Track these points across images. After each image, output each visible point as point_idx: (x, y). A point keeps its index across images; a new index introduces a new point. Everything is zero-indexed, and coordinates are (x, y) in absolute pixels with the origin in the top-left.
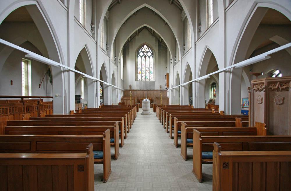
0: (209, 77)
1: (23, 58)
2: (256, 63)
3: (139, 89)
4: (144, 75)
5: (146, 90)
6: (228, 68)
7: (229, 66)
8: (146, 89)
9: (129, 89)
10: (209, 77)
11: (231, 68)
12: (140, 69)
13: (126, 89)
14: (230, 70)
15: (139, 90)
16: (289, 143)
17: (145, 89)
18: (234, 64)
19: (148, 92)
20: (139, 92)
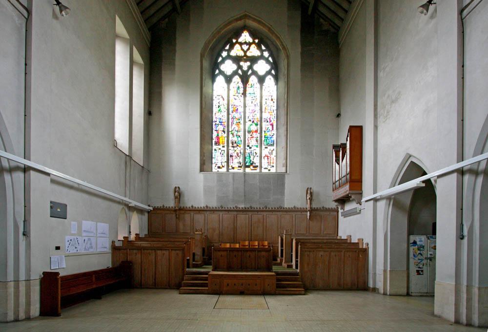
0: (424, 185)
3: (214, 204)
4: (240, 149)
5: (245, 211)
6: (465, 164)
7: (475, 155)
9: (171, 203)
10: (424, 185)
11: (479, 162)
12: (220, 128)
13: (159, 204)
14: (475, 167)
15: (213, 211)
17: (242, 206)
18: (399, 185)
19: (256, 217)
20: (214, 216)
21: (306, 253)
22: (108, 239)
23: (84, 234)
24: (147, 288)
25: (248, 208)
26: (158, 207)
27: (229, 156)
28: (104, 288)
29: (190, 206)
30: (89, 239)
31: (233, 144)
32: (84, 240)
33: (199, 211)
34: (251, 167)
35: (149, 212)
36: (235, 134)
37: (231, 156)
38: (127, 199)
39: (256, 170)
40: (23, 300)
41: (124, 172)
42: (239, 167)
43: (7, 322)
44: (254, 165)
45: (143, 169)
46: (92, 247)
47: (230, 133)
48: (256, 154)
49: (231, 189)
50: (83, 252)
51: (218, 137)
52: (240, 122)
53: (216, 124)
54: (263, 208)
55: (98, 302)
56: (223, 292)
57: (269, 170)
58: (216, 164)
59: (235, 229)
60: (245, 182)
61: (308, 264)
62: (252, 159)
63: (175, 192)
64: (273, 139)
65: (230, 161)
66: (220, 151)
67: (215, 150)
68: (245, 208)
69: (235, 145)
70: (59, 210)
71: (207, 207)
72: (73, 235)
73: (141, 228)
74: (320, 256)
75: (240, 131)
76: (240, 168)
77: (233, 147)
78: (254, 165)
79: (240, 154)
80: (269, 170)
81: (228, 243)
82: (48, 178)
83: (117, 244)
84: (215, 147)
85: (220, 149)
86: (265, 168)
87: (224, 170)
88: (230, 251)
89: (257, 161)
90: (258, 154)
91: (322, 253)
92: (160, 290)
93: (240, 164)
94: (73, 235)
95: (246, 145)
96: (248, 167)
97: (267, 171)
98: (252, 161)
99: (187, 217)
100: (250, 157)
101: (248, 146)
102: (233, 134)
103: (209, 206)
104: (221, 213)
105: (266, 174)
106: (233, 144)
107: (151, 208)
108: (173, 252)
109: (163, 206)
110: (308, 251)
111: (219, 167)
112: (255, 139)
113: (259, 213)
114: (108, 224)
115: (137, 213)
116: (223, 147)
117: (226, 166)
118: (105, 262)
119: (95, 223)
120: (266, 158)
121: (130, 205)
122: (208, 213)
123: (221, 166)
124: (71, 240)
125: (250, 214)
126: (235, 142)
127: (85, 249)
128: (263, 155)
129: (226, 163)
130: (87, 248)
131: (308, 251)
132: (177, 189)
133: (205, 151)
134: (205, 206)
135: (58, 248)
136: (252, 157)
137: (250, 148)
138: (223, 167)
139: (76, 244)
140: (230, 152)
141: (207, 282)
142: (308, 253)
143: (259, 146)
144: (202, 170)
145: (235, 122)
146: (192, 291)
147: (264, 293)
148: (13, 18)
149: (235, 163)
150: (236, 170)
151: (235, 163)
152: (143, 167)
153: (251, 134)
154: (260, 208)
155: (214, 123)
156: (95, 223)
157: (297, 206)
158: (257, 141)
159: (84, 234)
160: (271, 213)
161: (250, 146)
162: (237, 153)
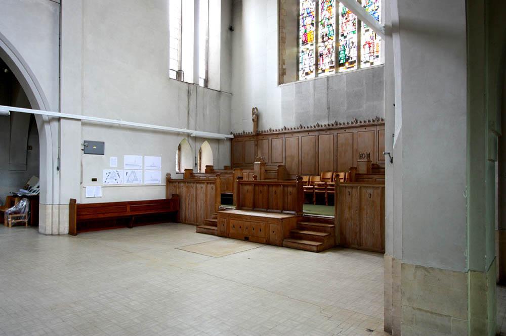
1: (334, 217)
2: (399, 13)
3: (292, 124)
4: (331, 43)
5: (328, 129)
8: (333, 122)
9: (250, 128)
12: (309, 20)
13: (240, 131)
15: (292, 133)
16: (257, 163)
17: (324, 123)
19: (343, 136)
20: (293, 141)
21: (347, 190)
22: (160, 171)
23: (126, 167)
24: (189, 224)
25: (333, 125)
26: (239, 134)
27: (319, 56)
28: (133, 218)
29: (268, 129)
30: (133, 172)
31: (323, 38)
32: (127, 173)
33: (278, 134)
34: (347, 64)
35: (231, 139)
36: (326, 24)
37: (321, 55)
38: (189, 131)
39: (353, 67)
40: (56, 219)
41: (186, 103)
42: (331, 67)
43: (46, 235)
44: (350, 60)
45: (220, 96)
46: (137, 180)
47: (320, 24)
48: (353, 43)
49: (311, 101)
50: (125, 183)
51: (305, 34)
52: (331, 5)
53: (303, 18)
54: (352, 123)
55: (129, 230)
56: (230, 235)
57: (372, 64)
58: (304, 70)
59: (316, 155)
60: (328, 88)
61: (350, 208)
62: (347, 53)
63: (253, 114)
64: (376, 15)
65: (320, 62)
66: (308, 51)
67: (303, 52)
68: (329, 125)
69: (326, 38)
70: (94, 148)
71: (285, 128)
72: (112, 168)
73: (216, 159)
74: (367, 195)
75: (331, 18)
76: (331, 70)
77: (324, 42)
78: (350, 60)
79: (332, 50)
80: (372, 64)
81: (306, 175)
82: (80, 123)
83: (173, 177)
84: (302, 48)
85: (308, 49)
86: (365, 63)
87: (312, 76)
88: (255, 185)
89: (353, 54)
90: (356, 44)
91: (370, 191)
92: (187, 226)
93: (332, 63)
94: (112, 168)
95: (340, 34)
96: (343, 65)
97: (368, 65)
98: (348, 55)
99: (265, 143)
100: (345, 50)
101: (343, 35)
102: (323, 25)
103: (304, 125)
104: (300, 135)
105: (366, 70)
106: (323, 38)
107: (232, 136)
108: (209, 185)
109: (244, 132)
110: (349, 187)
111: (307, 74)
112: (351, 23)
113: (347, 131)
114: (160, 158)
115: (208, 142)
116: (312, 45)
117: (314, 71)
118: (159, 194)
119: (142, 156)
120: (367, 45)
121: (192, 136)
122: (286, 136)
123: (309, 72)
124: (110, 173)
125: (335, 132)
126: (326, 35)
127: (128, 181)
128: (362, 43)
129: (314, 67)
130: (130, 180)
131: (349, 187)
132: (255, 110)
133: (285, 57)
134: (283, 127)
135: (94, 180)
136: (347, 49)
137: (345, 37)
138: (312, 72)
139: (115, 176)
140: (320, 50)
141: (216, 221)
142: (350, 190)
143: (356, 32)
144: (281, 82)
145: (325, 8)
146: (205, 230)
147: (269, 243)
148: (51, 7)
149: (326, 63)
150: (327, 73)
151: (326, 63)
152: (220, 91)
153: (346, 17)
154: (348, 123)
155: (301, 17)
156: (142, 156)
157: (288, 126)
158: (354, 25)
159: (126, 167)
160: (363, 129)
161: (345, 35)
162: (328, 49)
